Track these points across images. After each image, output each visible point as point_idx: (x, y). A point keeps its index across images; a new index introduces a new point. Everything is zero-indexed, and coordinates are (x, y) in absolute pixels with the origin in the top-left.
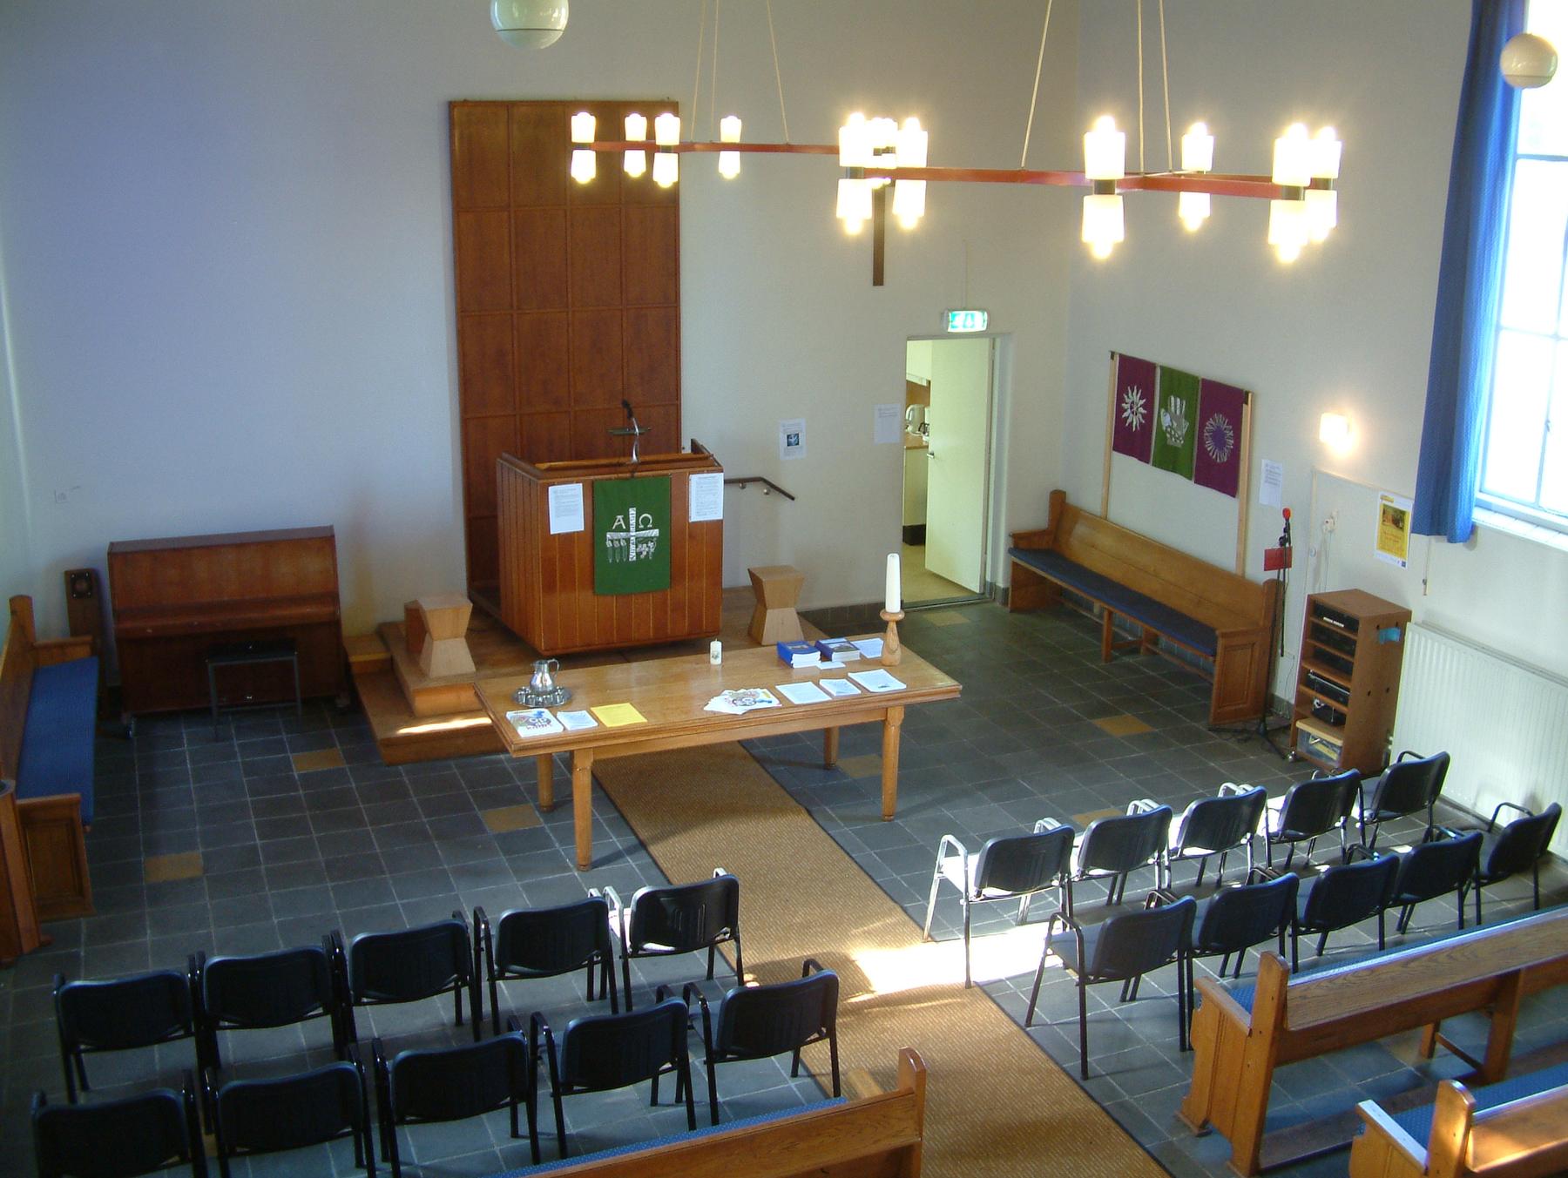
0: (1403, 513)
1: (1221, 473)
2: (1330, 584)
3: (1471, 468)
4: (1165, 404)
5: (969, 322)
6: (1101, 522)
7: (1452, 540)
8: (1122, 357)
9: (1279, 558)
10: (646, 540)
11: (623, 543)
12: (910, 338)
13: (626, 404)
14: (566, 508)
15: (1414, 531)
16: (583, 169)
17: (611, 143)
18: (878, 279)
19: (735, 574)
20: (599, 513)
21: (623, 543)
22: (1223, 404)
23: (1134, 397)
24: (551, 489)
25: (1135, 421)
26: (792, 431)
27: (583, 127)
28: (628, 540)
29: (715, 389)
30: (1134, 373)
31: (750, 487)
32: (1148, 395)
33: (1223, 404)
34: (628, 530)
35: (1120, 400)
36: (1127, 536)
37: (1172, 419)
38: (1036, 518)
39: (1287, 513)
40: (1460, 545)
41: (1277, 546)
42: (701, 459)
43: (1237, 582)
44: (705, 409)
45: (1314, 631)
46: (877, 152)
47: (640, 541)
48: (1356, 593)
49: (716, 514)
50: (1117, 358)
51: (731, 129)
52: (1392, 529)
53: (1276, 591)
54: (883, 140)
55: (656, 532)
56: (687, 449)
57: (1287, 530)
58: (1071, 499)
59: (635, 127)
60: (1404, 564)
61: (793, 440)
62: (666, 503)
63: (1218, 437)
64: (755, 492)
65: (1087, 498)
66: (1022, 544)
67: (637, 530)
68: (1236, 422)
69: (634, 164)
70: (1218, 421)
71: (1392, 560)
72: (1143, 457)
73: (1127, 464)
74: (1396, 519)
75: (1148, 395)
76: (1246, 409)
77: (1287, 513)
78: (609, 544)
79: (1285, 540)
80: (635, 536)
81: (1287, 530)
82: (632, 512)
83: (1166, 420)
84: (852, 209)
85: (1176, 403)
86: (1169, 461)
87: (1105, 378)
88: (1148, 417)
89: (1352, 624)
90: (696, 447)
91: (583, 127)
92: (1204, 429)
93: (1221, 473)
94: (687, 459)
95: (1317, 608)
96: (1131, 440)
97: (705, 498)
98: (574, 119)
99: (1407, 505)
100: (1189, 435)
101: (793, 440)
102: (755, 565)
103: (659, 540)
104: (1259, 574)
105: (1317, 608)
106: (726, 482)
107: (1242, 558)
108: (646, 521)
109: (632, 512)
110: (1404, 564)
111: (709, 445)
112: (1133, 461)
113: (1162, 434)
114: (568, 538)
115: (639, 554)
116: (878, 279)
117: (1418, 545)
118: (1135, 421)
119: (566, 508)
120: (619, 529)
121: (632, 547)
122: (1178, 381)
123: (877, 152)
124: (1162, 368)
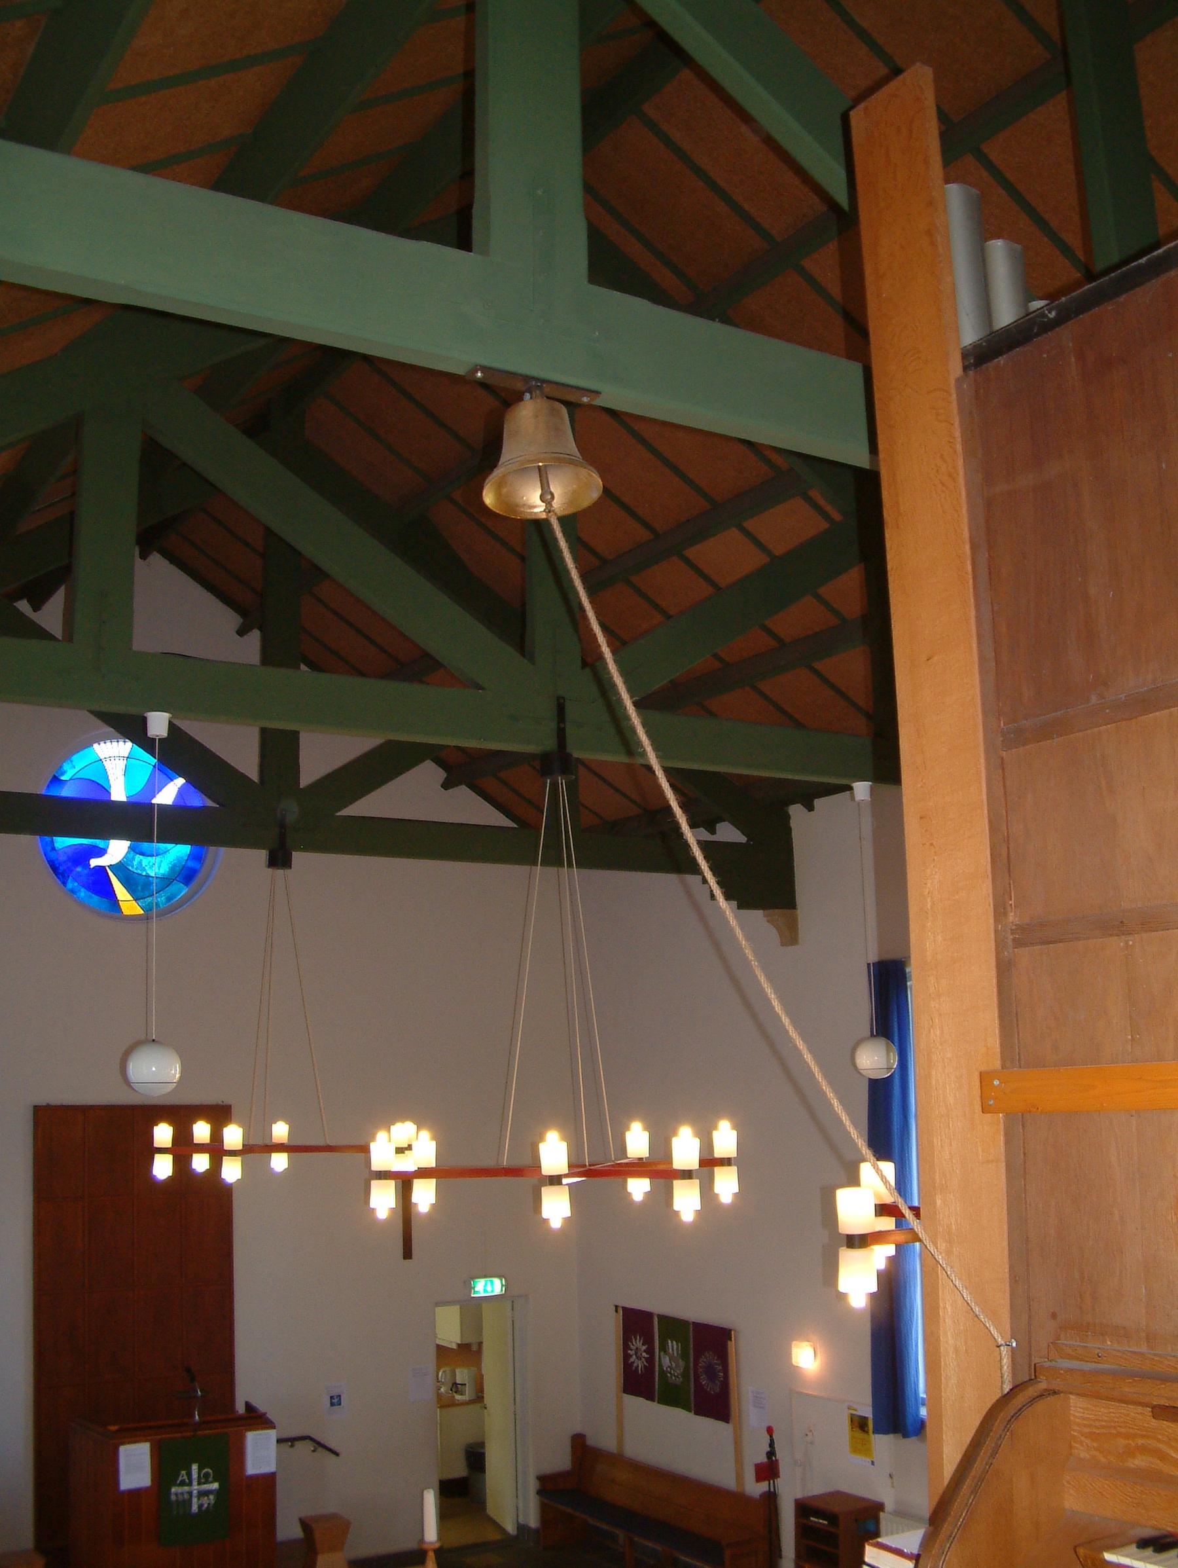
0: (866, 1418)
1: (715, 1402)
2: (816, 1488)
3: (913, 1372)
4: (663, 1348)
5: (489, 1288)
6: (617, 1459)
7: (906, 1435)
8: (624, 1309)
9: (768, 1470)
10: (206, 1493)
11: (186, 1496)
12: (437, 1304)
13: (188, 1370)
14: (135, 1465)
15: (876, 1431)
16: (163, 1167)
17: (183, 1147)
18: (408, 1253)
19: (288, 1529)
20: (166, 1469)
21: (186, 1496)
22: (712, 1342)
23: (638, 1343)
24: (122, 1449)
25: (640, 1364)
26: (335, 1392)
27: (163, 1134)
28: (190, 1493)
29: (262, 1366)
30: (635, 1322)
31: (299, 1445)
32: (649, 1341)
33: (712, 1342)
34: (190, 1484)
35: (626, 1347)
36: (638, 1468)
37: (670, 1359)
38: (560, 1460)
39: (770, 1430)
40: (914, 1438)
41: (766, 1460)
42: (256, 1419)
43: (738, 1498)
44: (252, 1383)
45: (804, 1531)
46: (400, 1150)
47: (201, 1494)
48: (837, 1495)
49: (269, 1467)
50: (621, 1311)
51: (280, 1131)
52: (859, 1434)
53: (771, 1499)
54: (404, 1145)
55: (216, 1486)
56: (240, 1408)
57: (772, 1444)
58: (591, 1442)
59: (201, 1131)
60: (873, 1463)
61: (335, 1400)
62: (225, 1459)
63: (711, 1372)
64: (303, 1448)
65: (604, 1440)
66: (549, 1486)
67: (199, 1483)
68: (723, 1355)
69: (201, 1163)
70: (708, 1357)
71: (860, 1460)
72: (649, 1397)
73: (635, 1404)
74: (860, 1424)
75: (649, 1341)
76: (731, 1345)
77: (770, 1430)
78: (173, 1498)
79: (771, 1453)
80: (197, 1489)
81: (772, 1444)
82: (195, 1467)
83: (666, 1361)
84: (383, 1200)
85: (673, 1346)
86: (671, 1397)
87: (611, 1328)
88: (650, 1360)
89: (833, 1518)
90: (248, 1406)
91: (163, 1134)
92: (687, 1361)
93: (715, 1402)
94: (241, 1418)
95: (804, 1509)
96: (637, 1382)
97: (260, 1453)
98: (156, 1128)
99: (867, 1411)
100: (685, 1374)
101: (335, 1400)
102: (307, 1511)
103: (218, 1493)
104: (756, 1489)
105: (804, 1509)
106: (279, 1441)
107: (739, 1477)
108: (207, 1475)
109: (195, 1467)
110: (873, 1463)
111: (261, 1405)
112: (641, 1400)
113: (663, 1373)
114: (135, 1493)
115: (200, 1507)
116: (408, 1253)
117: (883, 1443)
118: (640, 1364)
119: (135, 1465)
120: (183, 1483)
121: (195, 1500)
122: (673, 1326)
123: (400, 1150)
124: (659, 1316)
